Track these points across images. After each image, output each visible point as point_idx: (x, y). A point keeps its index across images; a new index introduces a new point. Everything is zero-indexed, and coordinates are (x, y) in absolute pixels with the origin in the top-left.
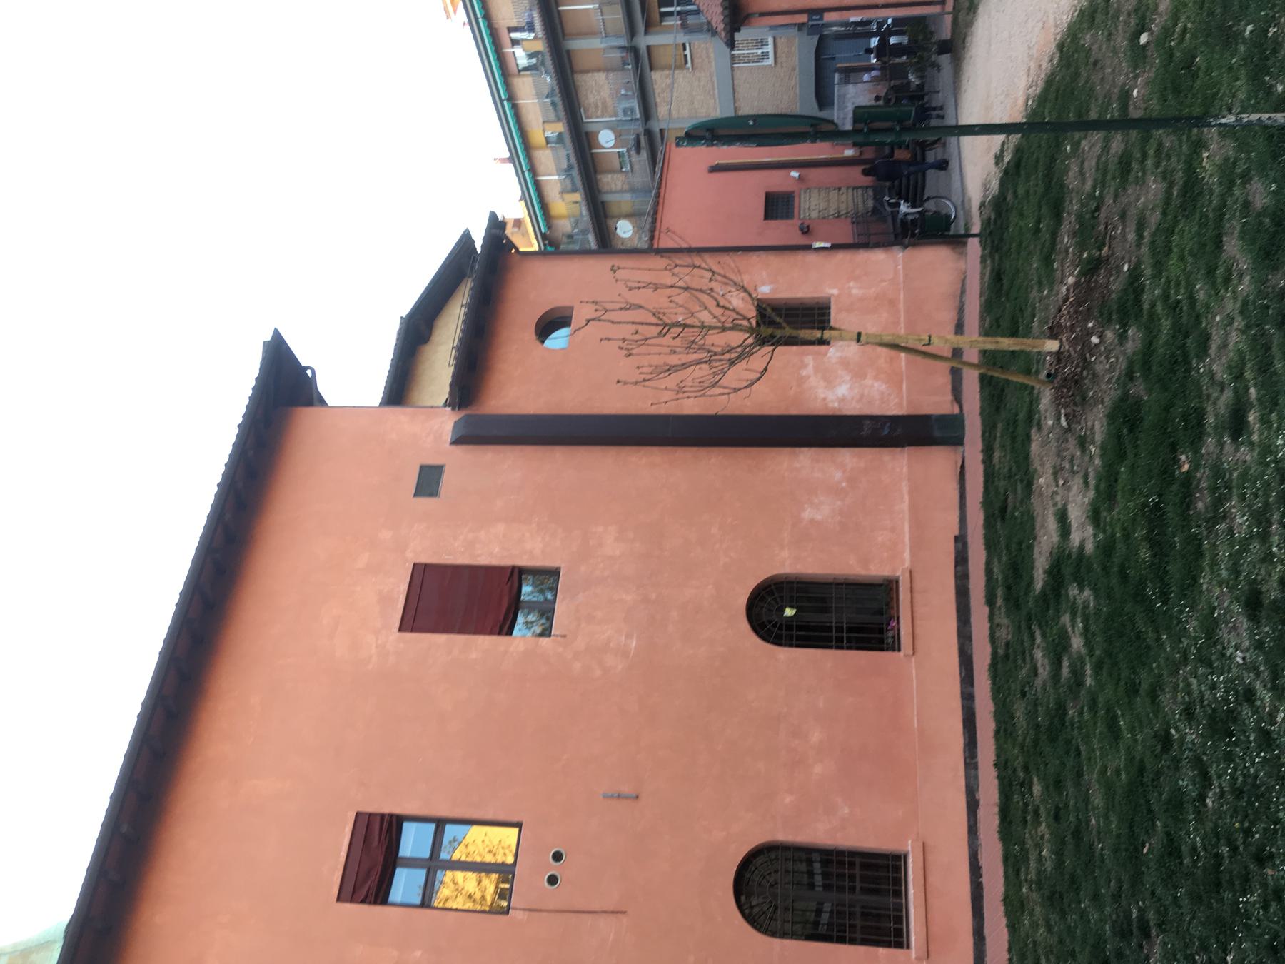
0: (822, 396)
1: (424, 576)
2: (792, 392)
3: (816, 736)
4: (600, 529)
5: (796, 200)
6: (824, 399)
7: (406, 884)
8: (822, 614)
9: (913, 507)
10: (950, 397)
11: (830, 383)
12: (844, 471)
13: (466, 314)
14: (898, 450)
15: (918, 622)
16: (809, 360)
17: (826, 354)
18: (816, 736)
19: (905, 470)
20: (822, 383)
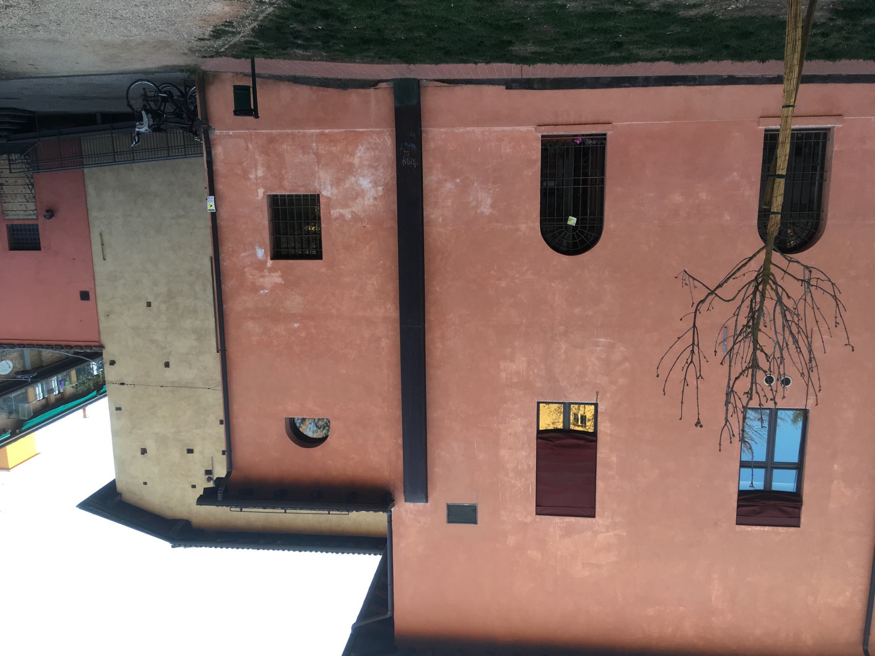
0: (371, 200)
1: (546, 504)
2: (368, 226)
3: (678, 198)
4: (503, 375)
5: (15, 223)
6: (375, 199)
7: (784, 482)
8: (573, 194)
9: (478, 123)
10: (371, 91)
11: (360, 194)
12: (446, 181)
13: (292, 508)
14: (424, 135)
15: (583, 120)
16: (335, 213)
17: (327, 198)
18: (678, 198)
19: (443, 130)
20: (359, 200)
